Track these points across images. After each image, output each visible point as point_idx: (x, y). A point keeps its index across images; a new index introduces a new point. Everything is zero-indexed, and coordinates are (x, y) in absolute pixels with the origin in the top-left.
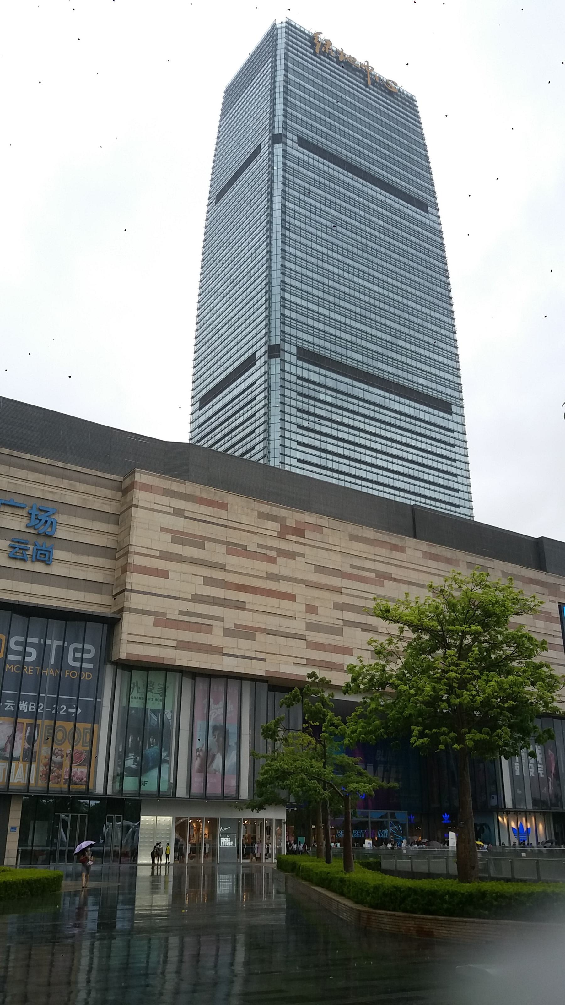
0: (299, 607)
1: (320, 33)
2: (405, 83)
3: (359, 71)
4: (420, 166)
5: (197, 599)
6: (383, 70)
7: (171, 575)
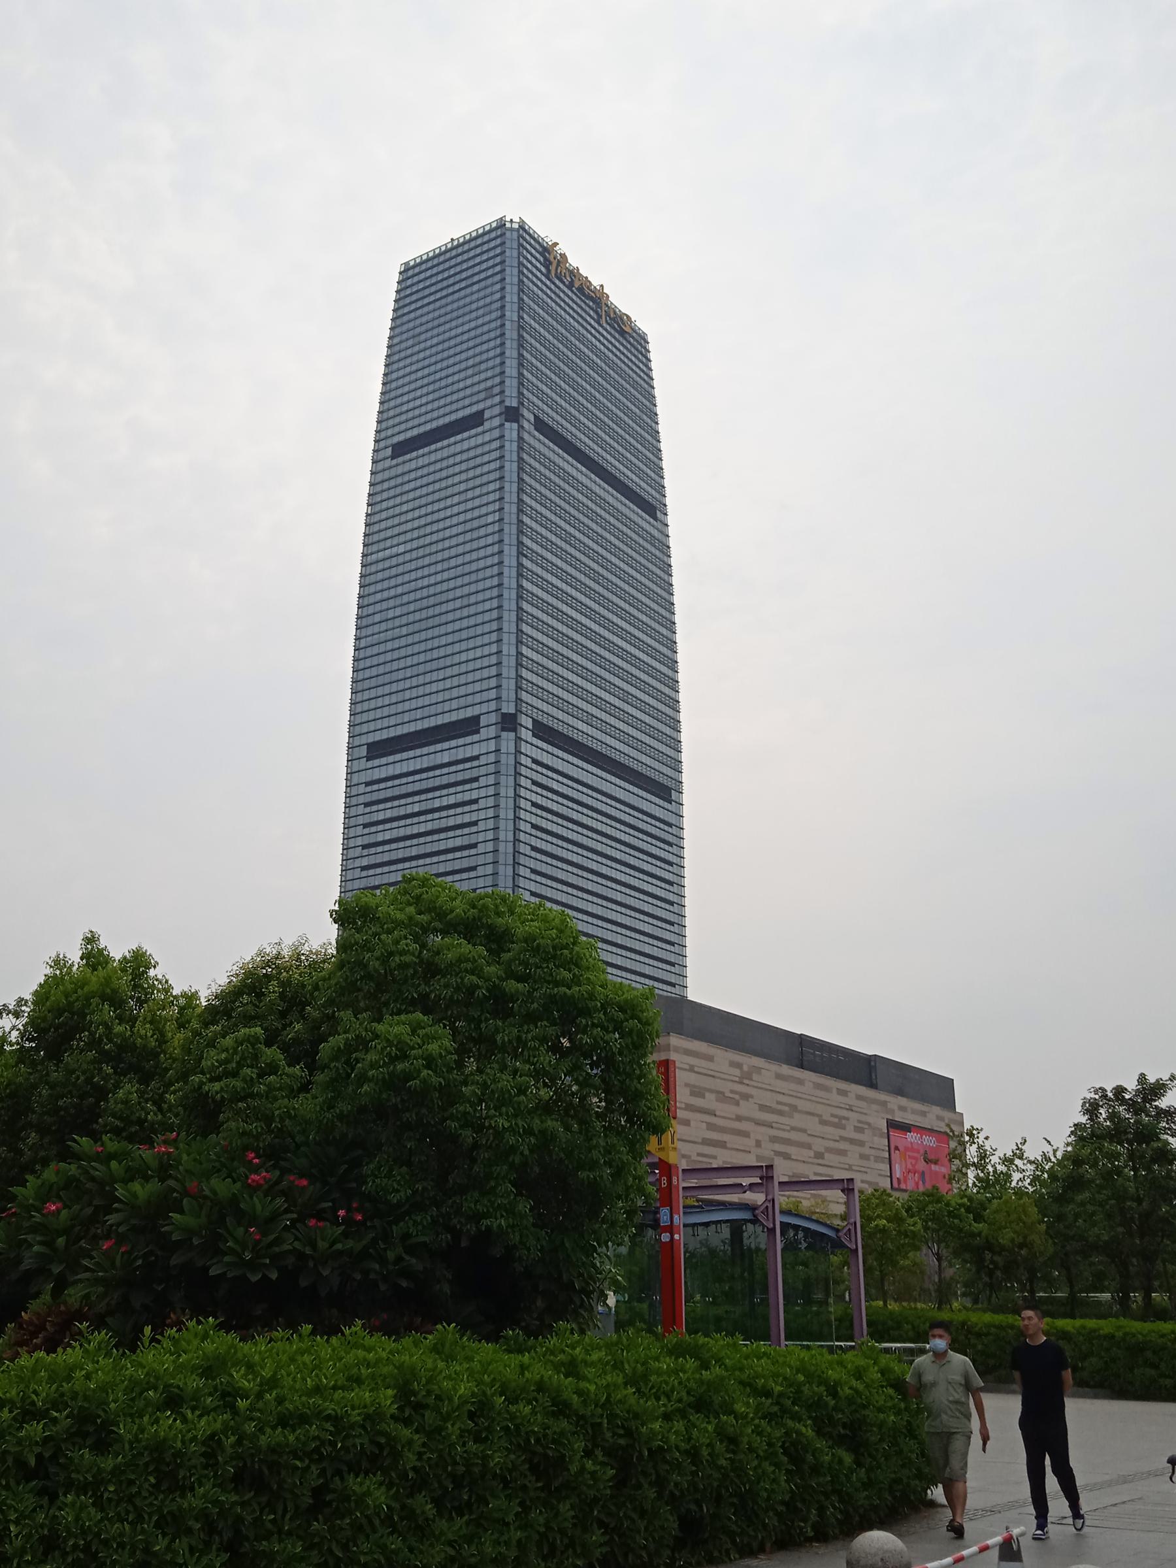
0: (750, 1143)
1: (556, 244)
2: (643, 323)
3: (591, 299)
4: (643, 442)
5: (706, 1142)
6: (620, 300)
7: (692, 1123)
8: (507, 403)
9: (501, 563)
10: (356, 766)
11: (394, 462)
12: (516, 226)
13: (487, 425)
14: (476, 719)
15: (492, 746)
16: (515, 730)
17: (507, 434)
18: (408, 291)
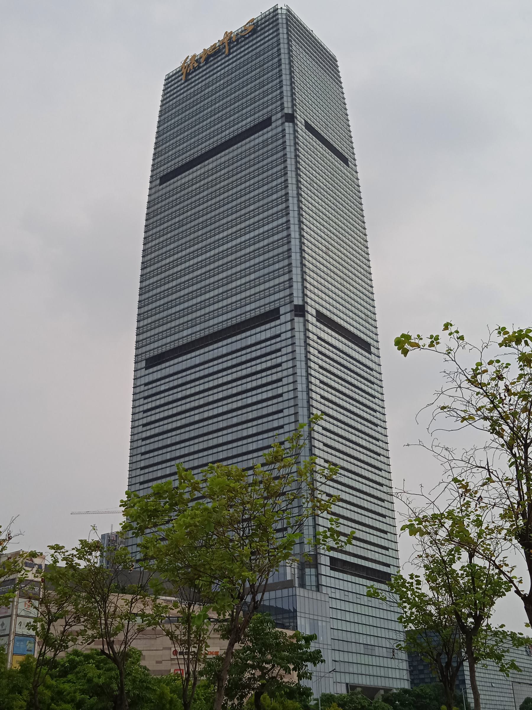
8: (296, 302)
9: (294, 374)
10: (139, 374)
11: (147, 372)
12: (284, 12)
13: (274, 125)
14: (277, 310)
15: (289, 326)
16: (303, 316)
17: (296, 326)
18: (169, 90)
